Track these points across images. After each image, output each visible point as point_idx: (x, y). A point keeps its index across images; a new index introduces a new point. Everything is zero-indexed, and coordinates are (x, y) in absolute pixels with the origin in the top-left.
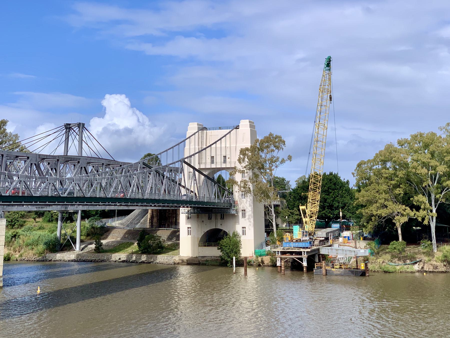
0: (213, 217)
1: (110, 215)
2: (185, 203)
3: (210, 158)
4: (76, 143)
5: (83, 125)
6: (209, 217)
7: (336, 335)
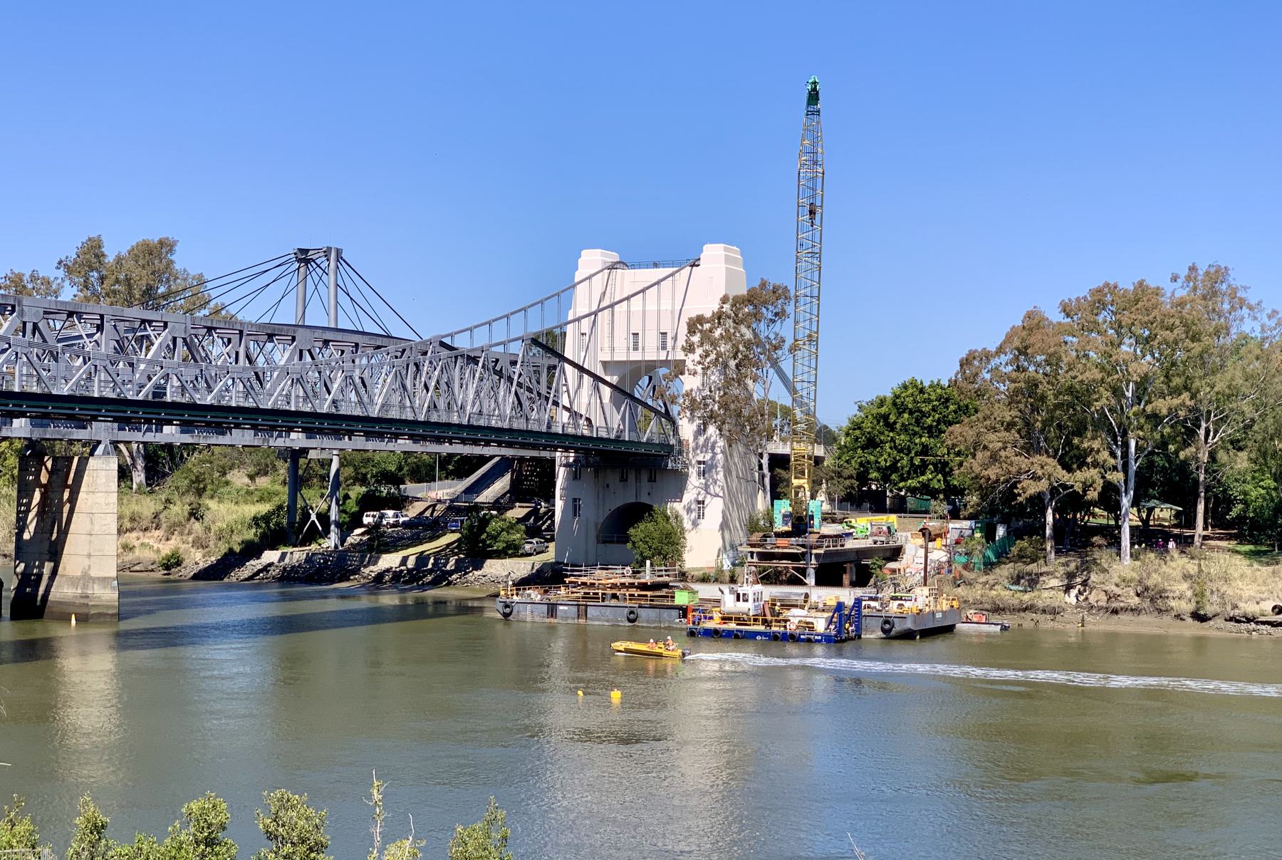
0: (632, 477)
1: (424, 473)
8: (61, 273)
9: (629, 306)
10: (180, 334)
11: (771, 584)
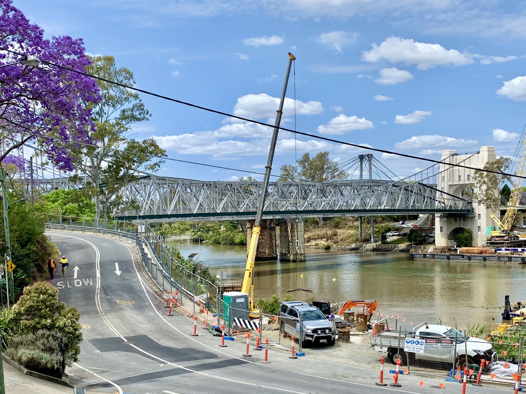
3: (458, 177)
4: (367, 165)
8: (298, 164)
11: (203, 131)
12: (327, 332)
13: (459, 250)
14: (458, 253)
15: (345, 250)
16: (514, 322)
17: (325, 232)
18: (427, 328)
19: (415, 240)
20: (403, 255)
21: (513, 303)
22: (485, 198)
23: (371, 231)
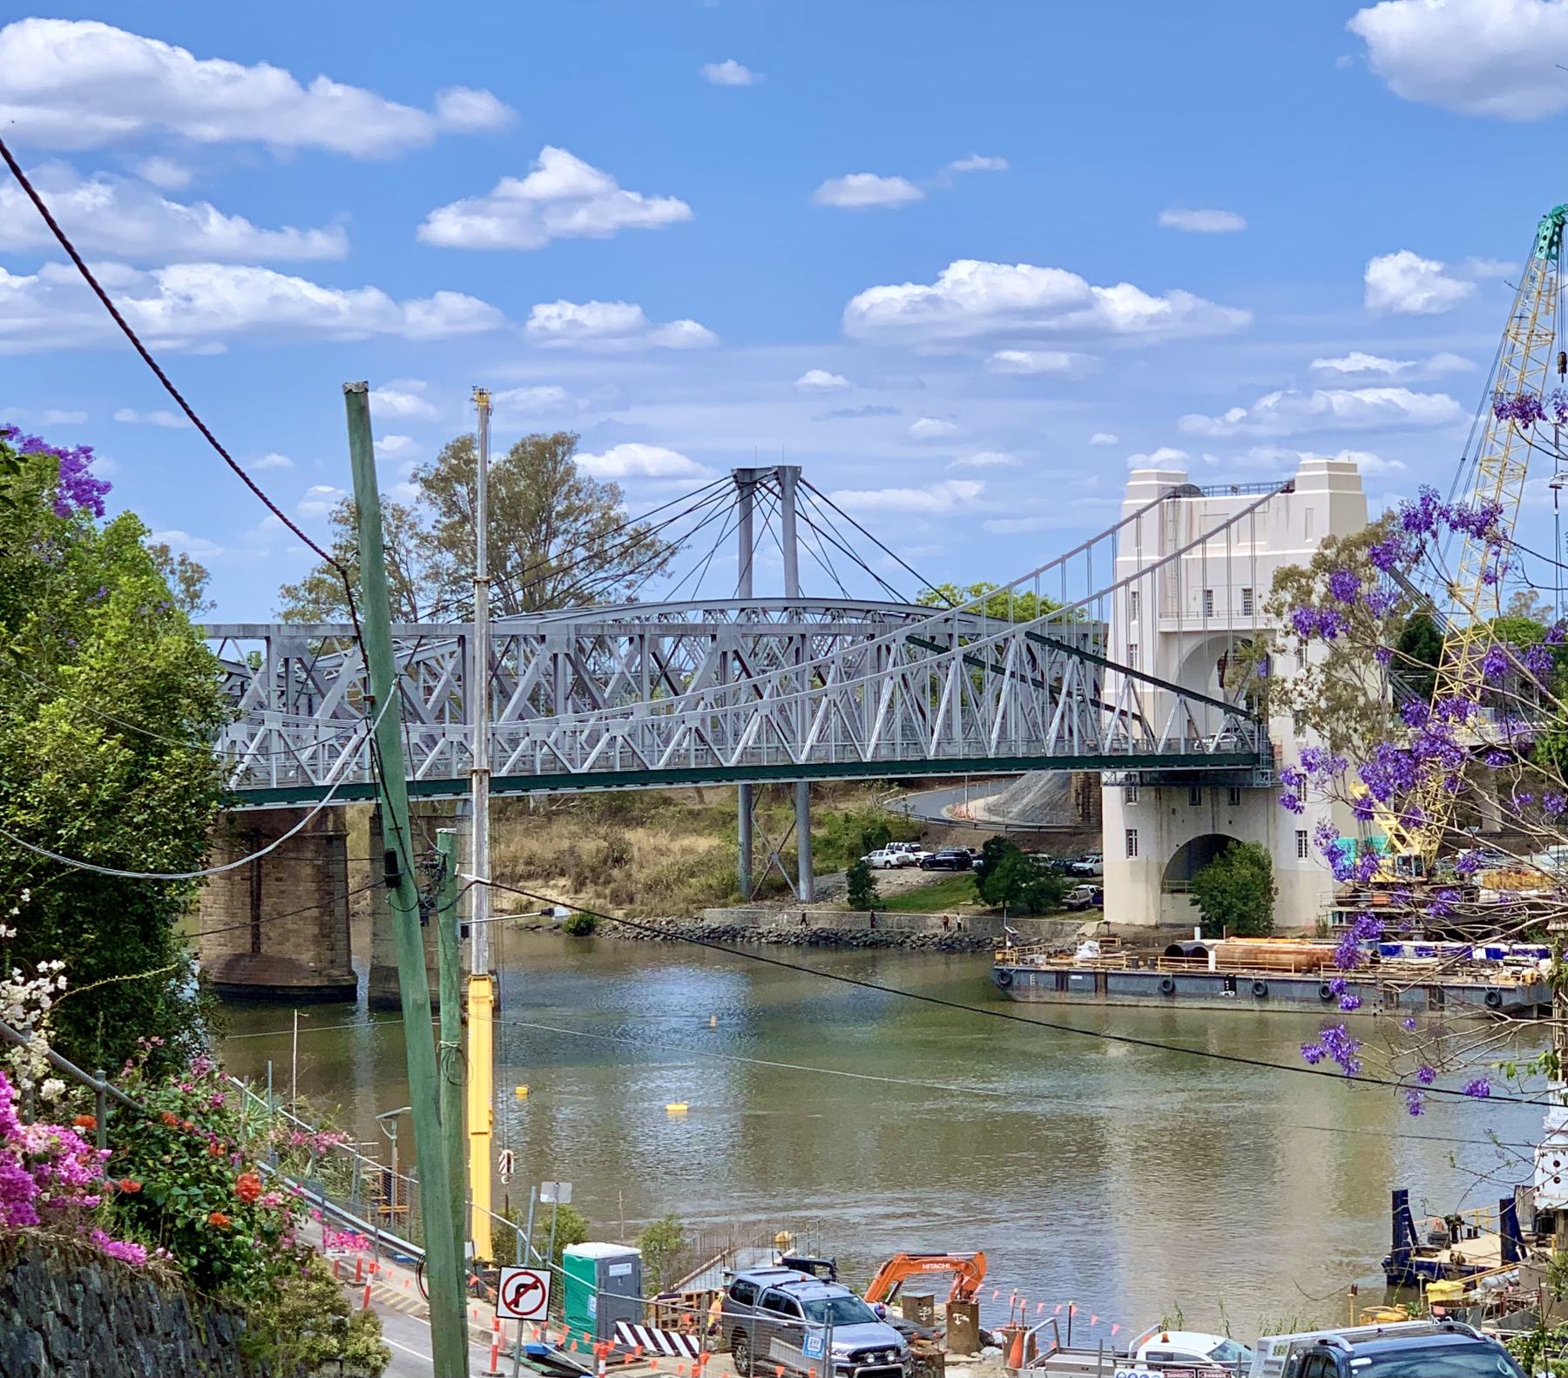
2: (1115, 761)
3: (1200, 596)
4: (776, 521)
5: (796, 471)
6: (1194, 798)
7: (1563, 738)
8: (417, 489)
9: (1204, 550)
10: (561, 651)
12: (891, 1358)
13: (1217, 949)
14: (1212, 967)
15: (671, 938)
16: (1432, 1298)
17: (566, 844)
18: (1165, 1340)
19: (1012, 893)
20: (961, 969)
21: (1425, 1225)
22: (1323, 704)
23: (795, 841)
